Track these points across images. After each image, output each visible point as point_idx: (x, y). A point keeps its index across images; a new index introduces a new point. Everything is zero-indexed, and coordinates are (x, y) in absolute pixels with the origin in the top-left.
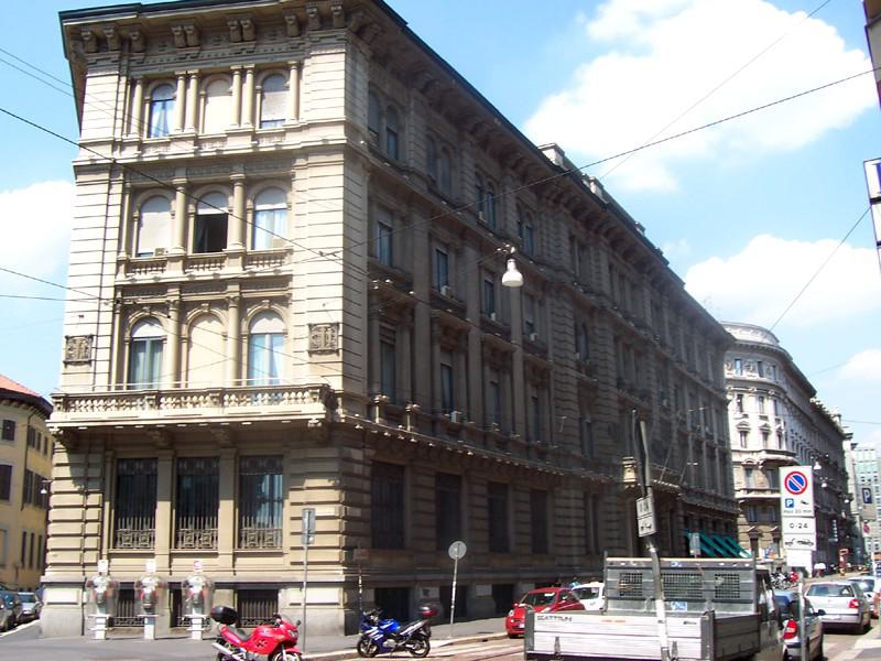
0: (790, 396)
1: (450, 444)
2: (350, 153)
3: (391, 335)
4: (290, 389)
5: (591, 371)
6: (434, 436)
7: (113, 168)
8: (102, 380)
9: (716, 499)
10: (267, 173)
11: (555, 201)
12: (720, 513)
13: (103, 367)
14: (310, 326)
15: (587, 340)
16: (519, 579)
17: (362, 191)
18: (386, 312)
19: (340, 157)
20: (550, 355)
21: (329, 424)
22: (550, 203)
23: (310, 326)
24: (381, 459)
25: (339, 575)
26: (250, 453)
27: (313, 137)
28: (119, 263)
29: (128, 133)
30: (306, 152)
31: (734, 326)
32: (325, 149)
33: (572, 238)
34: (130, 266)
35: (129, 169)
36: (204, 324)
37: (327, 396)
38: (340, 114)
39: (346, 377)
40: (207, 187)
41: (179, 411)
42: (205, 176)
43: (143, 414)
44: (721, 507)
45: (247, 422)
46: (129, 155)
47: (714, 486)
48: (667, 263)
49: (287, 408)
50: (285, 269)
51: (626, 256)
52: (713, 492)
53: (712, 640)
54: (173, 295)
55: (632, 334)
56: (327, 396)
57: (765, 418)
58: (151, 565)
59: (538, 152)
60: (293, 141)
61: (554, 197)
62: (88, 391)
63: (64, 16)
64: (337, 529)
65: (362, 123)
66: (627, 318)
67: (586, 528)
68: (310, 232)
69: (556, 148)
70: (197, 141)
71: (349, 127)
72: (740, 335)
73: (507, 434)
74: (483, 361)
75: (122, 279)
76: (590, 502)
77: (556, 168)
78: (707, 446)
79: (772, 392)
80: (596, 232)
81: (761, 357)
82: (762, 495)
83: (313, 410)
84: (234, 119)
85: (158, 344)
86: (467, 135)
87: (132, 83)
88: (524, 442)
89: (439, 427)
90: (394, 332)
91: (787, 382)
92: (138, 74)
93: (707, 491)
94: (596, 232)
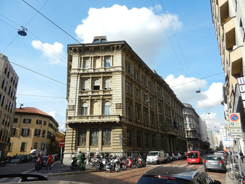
1: (139, 126)
2: (123, 72)
4: (112, 116)
5: (161, 112)
8: (76, 113)
9: (183, 137)
10: (107, 75)
11: (155, 81)
12: (184, 140)
13: (77, 111)
14: (116, 104)
15: (160, 106)
16: (143, 152)
17: (124, 79)
18: (129, 102)
19: (121, 73)
21: (120, 122)
22: (154, 81)
23: (116, 104)
24: (128, 129)
25: (122, 151)
26: (105, 128)
27: (117, 69)
28: (79, 92)
29: (81, 67)
30: (114, 72)
31: (184, 104)
32: (118, 71)
33: (157, 87)
34: (82, 93)
36: (96, 103)
37: (120, 117)
38: (121, 65)
39: (123, 113)
41: (92, 119)
42: (95, 76)
43: (85, 120)
44: (184, 139)
45: (80, 122)
46: (81, 72)
47: (182, 135)
49: (112, 119)
50: (111, 93)
51: (166, 90)
54: (101, 97)
55: (168, 105)
56: (120, 117)
57: (190, 122)
58: (97, 149)
59: (152, 71)
60: (112, 70)
62: (74, 116)
63: (68, 45)
65: (124, 67)
66: (167, 102)
67: (161, 142)
68: (116, 86)
69: (155, 71)
70: (94, 69)
71: (122, 68)
72: (186, 106)
74: (144, 110)
76: (162, 137)
77: (155, 75)
81: (189, 110)
82: (190, 137)
83: (117, 119)
84: (101, 66)
85: (86, 108)
87: (81, 58)
88: (150, 125)
91: (194, 115)
92: (83, 56)
93: (181, 136)
94: (161, 87)
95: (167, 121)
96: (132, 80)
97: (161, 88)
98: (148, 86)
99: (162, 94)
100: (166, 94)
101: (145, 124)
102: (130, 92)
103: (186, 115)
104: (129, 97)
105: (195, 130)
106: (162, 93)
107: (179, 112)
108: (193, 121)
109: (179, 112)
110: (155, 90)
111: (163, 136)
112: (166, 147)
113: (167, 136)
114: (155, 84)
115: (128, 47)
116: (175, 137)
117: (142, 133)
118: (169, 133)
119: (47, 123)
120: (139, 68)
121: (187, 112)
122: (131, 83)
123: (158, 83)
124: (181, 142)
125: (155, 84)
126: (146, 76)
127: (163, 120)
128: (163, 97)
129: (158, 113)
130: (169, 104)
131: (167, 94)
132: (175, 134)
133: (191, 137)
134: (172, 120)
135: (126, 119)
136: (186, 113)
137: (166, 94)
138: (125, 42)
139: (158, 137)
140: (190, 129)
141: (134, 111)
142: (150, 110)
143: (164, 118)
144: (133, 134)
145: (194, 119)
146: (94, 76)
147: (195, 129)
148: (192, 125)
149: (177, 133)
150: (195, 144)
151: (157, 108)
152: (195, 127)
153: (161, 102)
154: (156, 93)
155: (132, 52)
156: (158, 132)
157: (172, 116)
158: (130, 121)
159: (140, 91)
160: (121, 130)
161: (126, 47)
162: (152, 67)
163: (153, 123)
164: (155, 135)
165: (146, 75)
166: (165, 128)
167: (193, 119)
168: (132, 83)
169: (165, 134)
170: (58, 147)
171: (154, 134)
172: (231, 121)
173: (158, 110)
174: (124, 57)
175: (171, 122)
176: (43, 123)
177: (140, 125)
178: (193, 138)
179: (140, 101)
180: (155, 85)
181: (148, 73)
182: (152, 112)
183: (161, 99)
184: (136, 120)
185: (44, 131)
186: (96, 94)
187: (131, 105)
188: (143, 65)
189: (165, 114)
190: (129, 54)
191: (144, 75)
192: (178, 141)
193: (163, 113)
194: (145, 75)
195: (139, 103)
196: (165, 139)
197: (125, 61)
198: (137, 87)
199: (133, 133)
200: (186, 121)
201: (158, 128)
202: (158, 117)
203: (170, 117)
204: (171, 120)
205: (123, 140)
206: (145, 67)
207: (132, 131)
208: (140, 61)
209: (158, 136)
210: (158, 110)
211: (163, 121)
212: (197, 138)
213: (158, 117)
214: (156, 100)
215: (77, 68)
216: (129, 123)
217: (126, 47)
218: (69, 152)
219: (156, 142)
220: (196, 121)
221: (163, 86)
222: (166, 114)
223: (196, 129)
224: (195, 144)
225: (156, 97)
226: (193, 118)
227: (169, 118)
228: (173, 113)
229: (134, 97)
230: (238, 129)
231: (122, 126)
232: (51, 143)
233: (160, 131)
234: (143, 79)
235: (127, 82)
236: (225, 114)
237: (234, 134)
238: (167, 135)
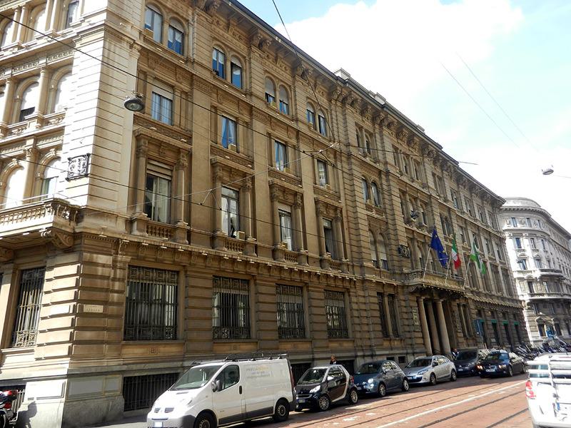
0: (553, 237)
3: (169, 173)
6: (213, 248)
11: (342, 102)
14: (69, 159)
16: (356, 356)
20: (342, 198)
22: (339, 104)
24: (137, 263)
33: (434, 175)
40: (28, 80)
47: (499, 289)
48: (441, 147)
51: (410, 142)
52: (499, 294)
53: (342, 408)
61: (341, 98)
64: (67, 312)
69: (342, 70)
73: (299, 250)
77: (344, 82)
78: (491, 264)
79: (539, 234)
80: (381, 125)
82: (541, 297)
86: (297, 78)
88: (318, 256)
89: (280, 255)
90: (172, 171)
93: (494, 293)
94: (381, 125)
97: (381, 133)
108: (547, 249)
111: (387, 296)
112: (408, 335)
116: (456, 295)
120: (482, 200)
121: (521, 223)
127: (392, 237)
129: (362, 212)
130: (425, 186)
133: (546, 297)
136: (519, 226)
140: (537, 274)
141: (491, 277)
145: (551, 242)
146: (17, 73)
148: (544, 261)
150: (562, 317)
153: (380, 178)
156: (364, 281)
160: (72, 269)
161: (308, 67)
162: (331, 59)
166: (401, 267)
167: (546, 243)
171: (339, 291)
177: (479, 296)
178: (550, 299)
181: (462, 182)
183: (380, 166)
188: (304, 66)
190: (279, 55)
194: (456, 185)
196: (403, 303)
199: (308, 294)
200: (524, 250)
205: (78, 313)
206: (274, 41)
207: (252, 283)
208: (240, 17)
209: (361, 293)
211: (393, 242)
220: (563, 252)
221: (350, 101)
223: (561, 272)
224: (562, 317)
226: (545, 237)
231: (81, 253)
233: (368, 276)
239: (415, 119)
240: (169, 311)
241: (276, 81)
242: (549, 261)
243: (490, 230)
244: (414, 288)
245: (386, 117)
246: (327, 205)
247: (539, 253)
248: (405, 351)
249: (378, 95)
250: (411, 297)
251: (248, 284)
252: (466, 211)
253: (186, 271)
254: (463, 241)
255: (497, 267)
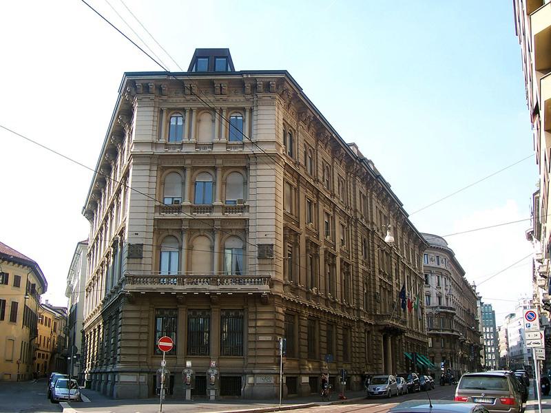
5: (368, 265)
7: (152, 156)
9: (418, 334)
10: (243, 165)
33: (361, 192)
35: (161, 157)
74: (325, 261)
75: (157, 216)
77: (357, 158)
82: (437, 332)
86: (301, 123)
87: (161, 111)
88: (340, 302)
95: (382, 290)
96: (298, 177)
98: (336, 193)
99: (371, 212)
100: (381, 212)
101: (327, 300)
102: (294, 213)
103: (430, 271)
104: (292, 226)
105: (452, 311)
106: (371, 209)
107: (414, 261)
109: (414, 261)
110: (355, 202)
113: (380, 331)
114: (354, 185)
115: (294, 87)
116: (401, 332)
117: (351, 331)
118: (389, 322)
119: (23, 283)
122: (295, 184)
123: (362, 181)
124: (412, 345)
125: (354, 185)
126: (333, 163)
128: (375, 221)
131: (385, 211)
132: (181, 287)
134: (394, 286)
135: (284, 285)
137: (381, 212)
138: (285, 72)
139: (357, 334)
141: (303, 263)
142: (307, 240)
143: (374, 280)
144: (320, 329)
147: (451, 309)
149: (404, 323)
151: (357, 254)
152: (451, 305)
153: (368, 236)
154: (356, 211)
155: (324, 124)
156: (360, 321)
157: (394, 275)
158: (294, 290)
159: (317, 205)
162: (347, 135)
163: (345, 294)
164: (350, 327)
165: (333, 158)
168: (298, 185)
169: (376, 325)
170: (38, 352)
172: (527, 322)
173: (361, 257)
174: (280, 112)
175: (391, 292)
176: (11, 280)
177: (334, 308)
179: (298, 225)
180: (354, 188)
182: (345, 264)
183: (369, 227)
184: (307, 288)
185: (15, 305)
186: (202, 214)
187: (295, 247)
189: (377, 271)
191: (312, 141)
192: (406, 343)
193: (374, 267)
195: (315, 240)
197: (283, 124)
198: (310, 195)
199: (336, 331)
201: (359, 310)
202: (361, 279)
203: (390, 278)
204: (391, 286)
206: (315, 117)
209: (357, 330)
210: (361, 257)
212: (455, 333)
213: (361, 279)
214: (356, 232)
215: (149, 139)
216: (291, 297)
217: (289, 87)
218: (133, 370)
219: (352, 346)
222: (379, 269)
225: (357, 220)
227: (387, 281)
228: (397, 265)
229: (302, 226)
230: (536, 333)
232: (30, 341)
234: (324, 171)
235: (287, 182)
236: (534, 266)
237: (530, 341)
238: (381, 328)
239: (367, 154)
240: (159, 327)
241: (287, 126)
242: (447, 299)
243: (335, 201)
244: (383, 327)
245: (361, 169)
246: (291, 230)
247: (441, 291)
248: (299, 372)
249: (354, 145)
250: (380, 334)
251: (294, 318)
252: (321, 180)
253: (299, 316)
254: (327, 234)
255: (334, 256)
